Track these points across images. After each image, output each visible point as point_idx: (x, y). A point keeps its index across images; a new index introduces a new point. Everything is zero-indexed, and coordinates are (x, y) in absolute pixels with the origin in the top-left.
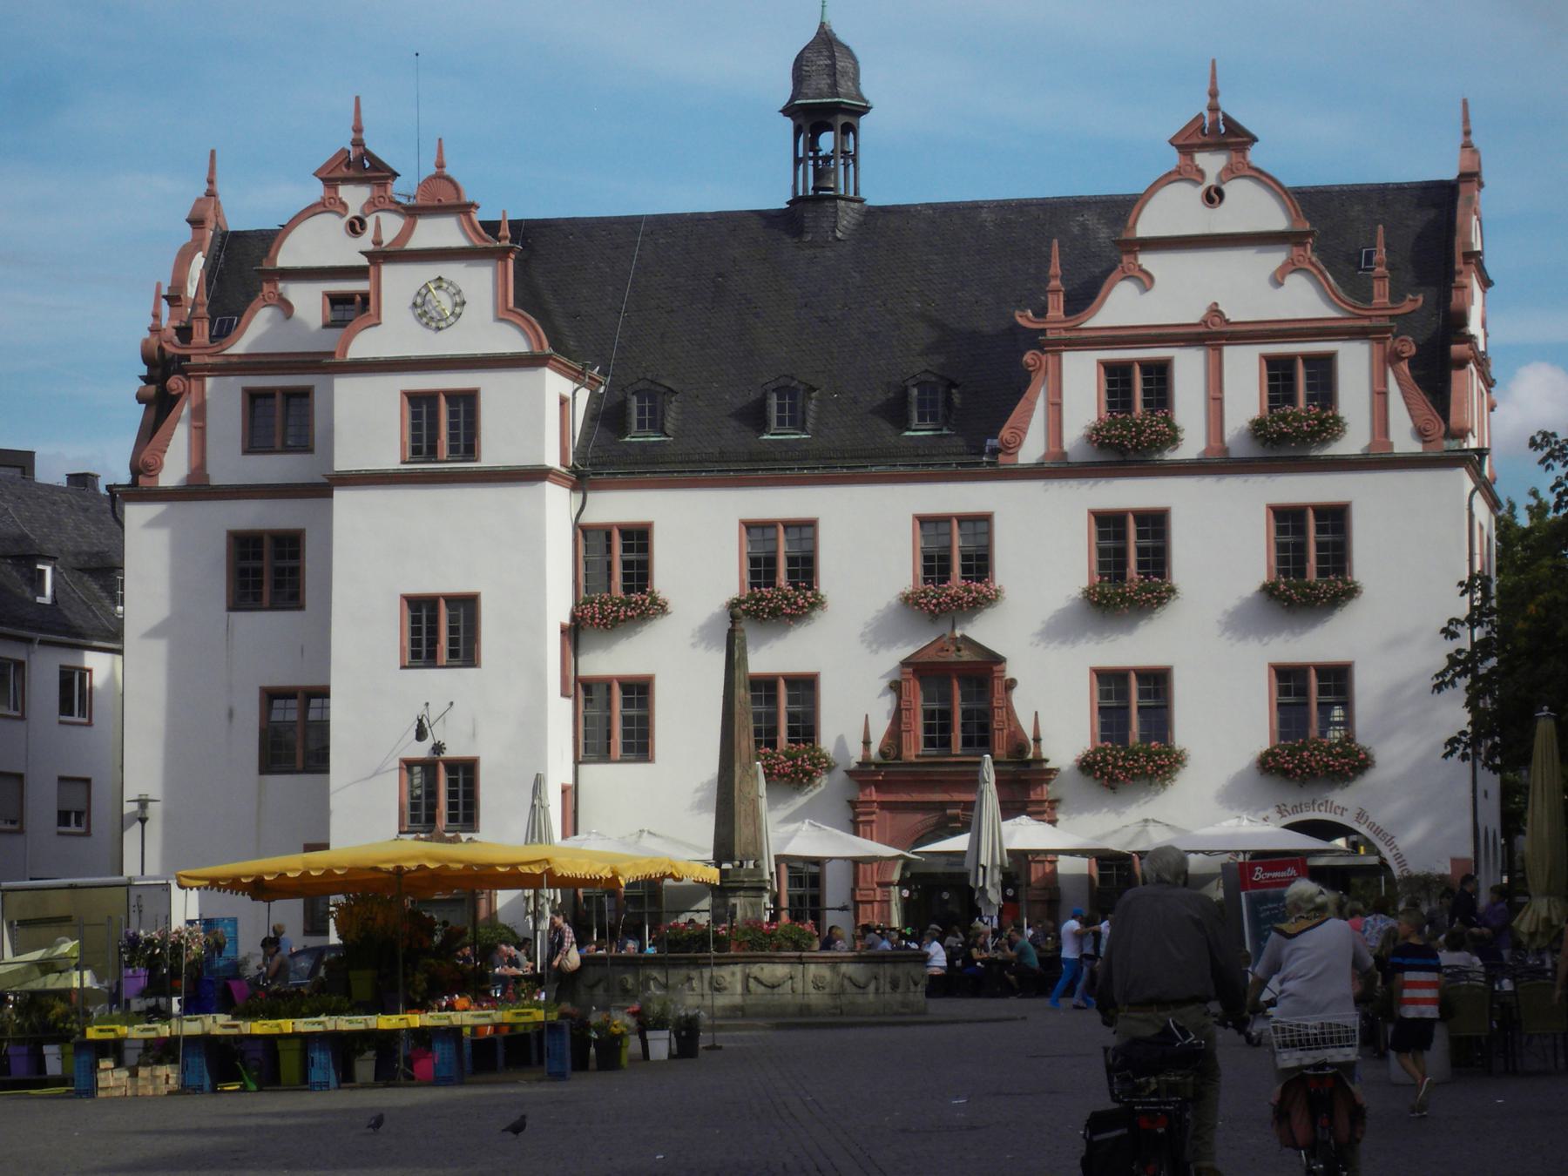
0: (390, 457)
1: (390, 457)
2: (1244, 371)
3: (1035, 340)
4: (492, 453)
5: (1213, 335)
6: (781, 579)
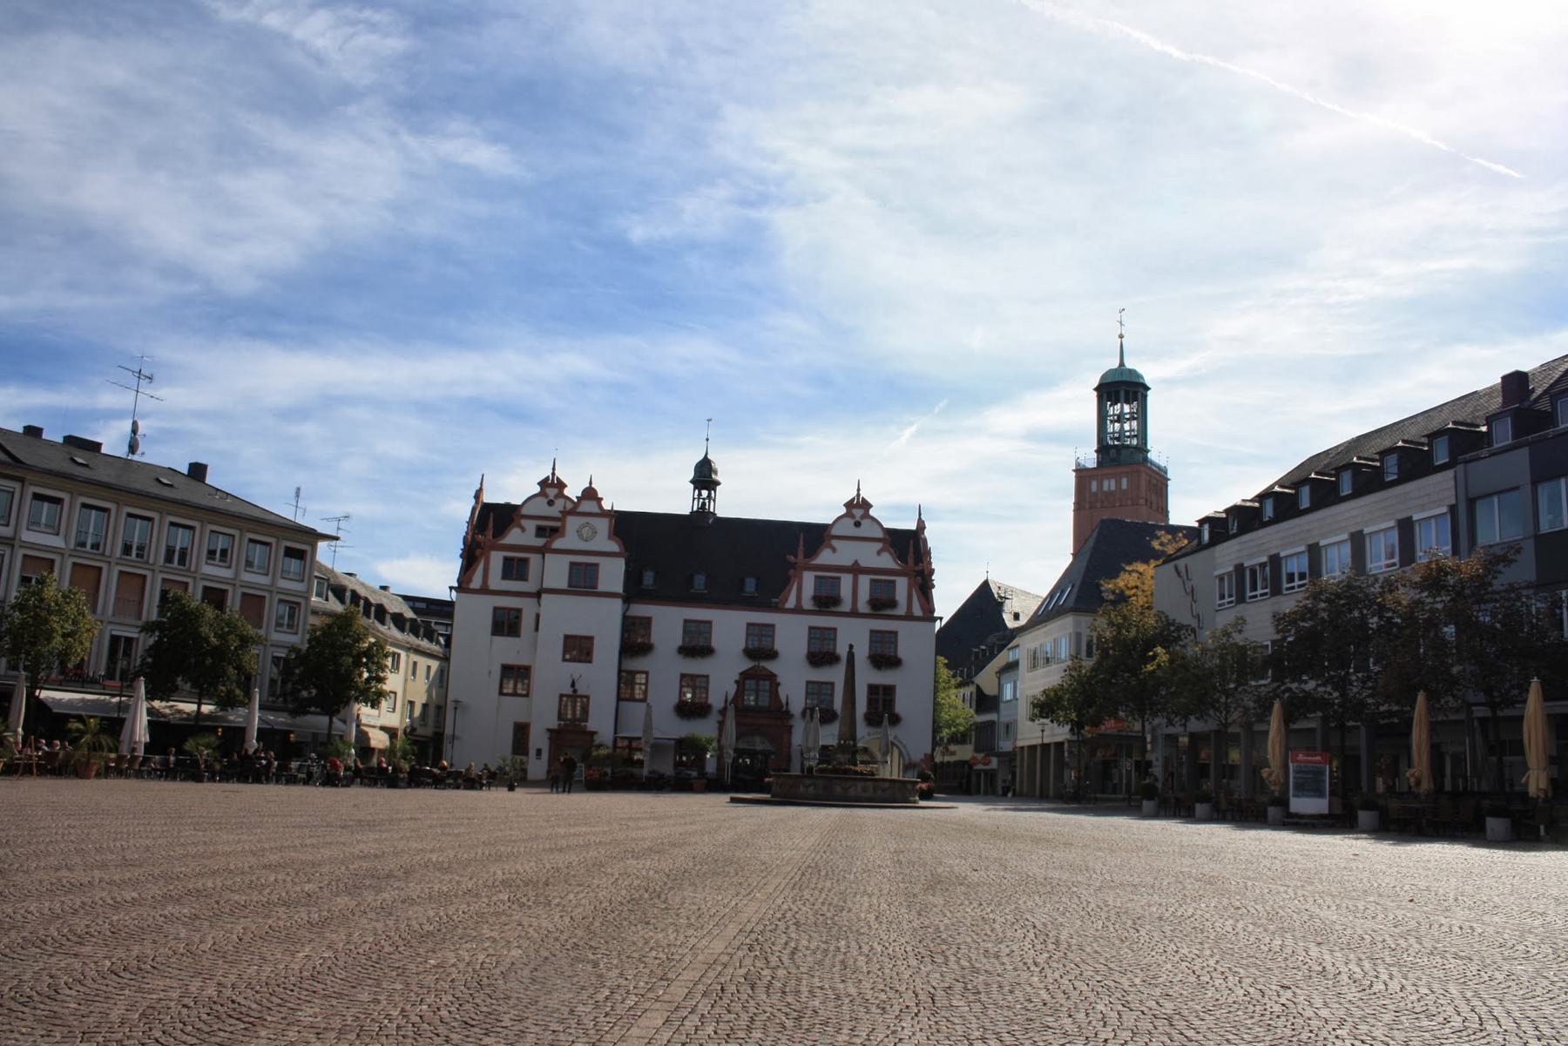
0: (563, 584)
1: (564, 585)
2: (865, 581)
3: (793, 566)
5: (856, 570)
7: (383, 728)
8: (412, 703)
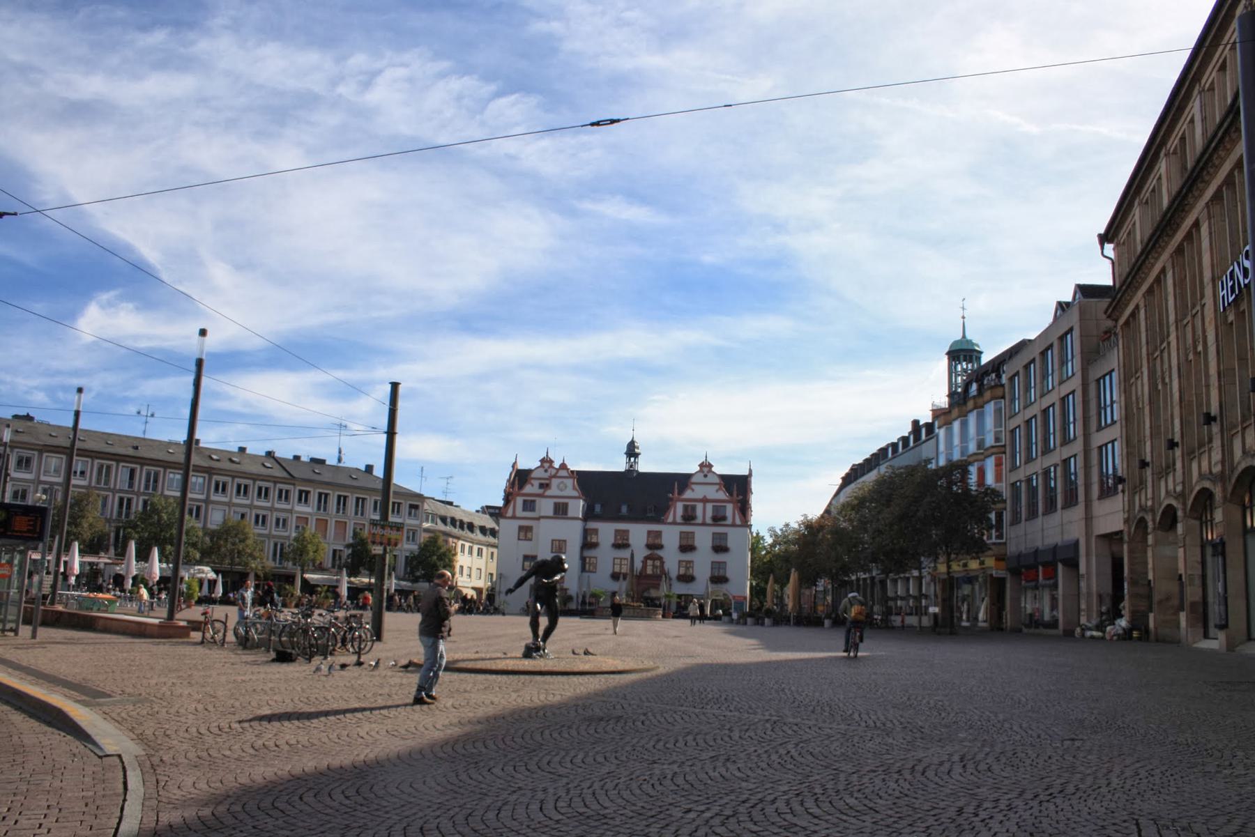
0: (551, 513)
2: (709, 506)
3: (671, 499)
4: (570, 514)
5: (705, 500)
6: (621, 543)
7: (473, 588)
8: (491, 575)
